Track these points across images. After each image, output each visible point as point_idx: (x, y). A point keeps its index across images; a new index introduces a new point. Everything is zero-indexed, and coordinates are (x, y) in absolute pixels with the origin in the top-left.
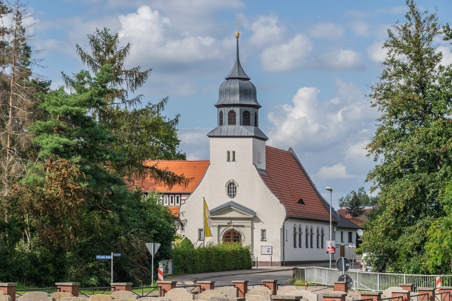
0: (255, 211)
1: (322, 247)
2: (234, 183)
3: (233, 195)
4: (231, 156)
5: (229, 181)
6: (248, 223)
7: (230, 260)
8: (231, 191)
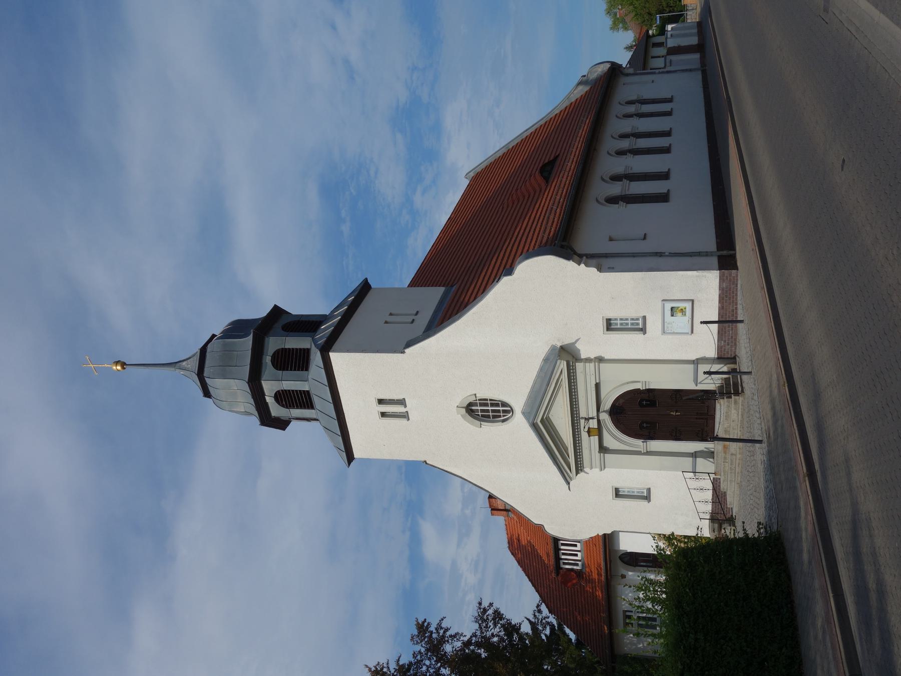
1: (670, 100)
4: (392, 408)
6: (585, 376)
8: (493, 411)
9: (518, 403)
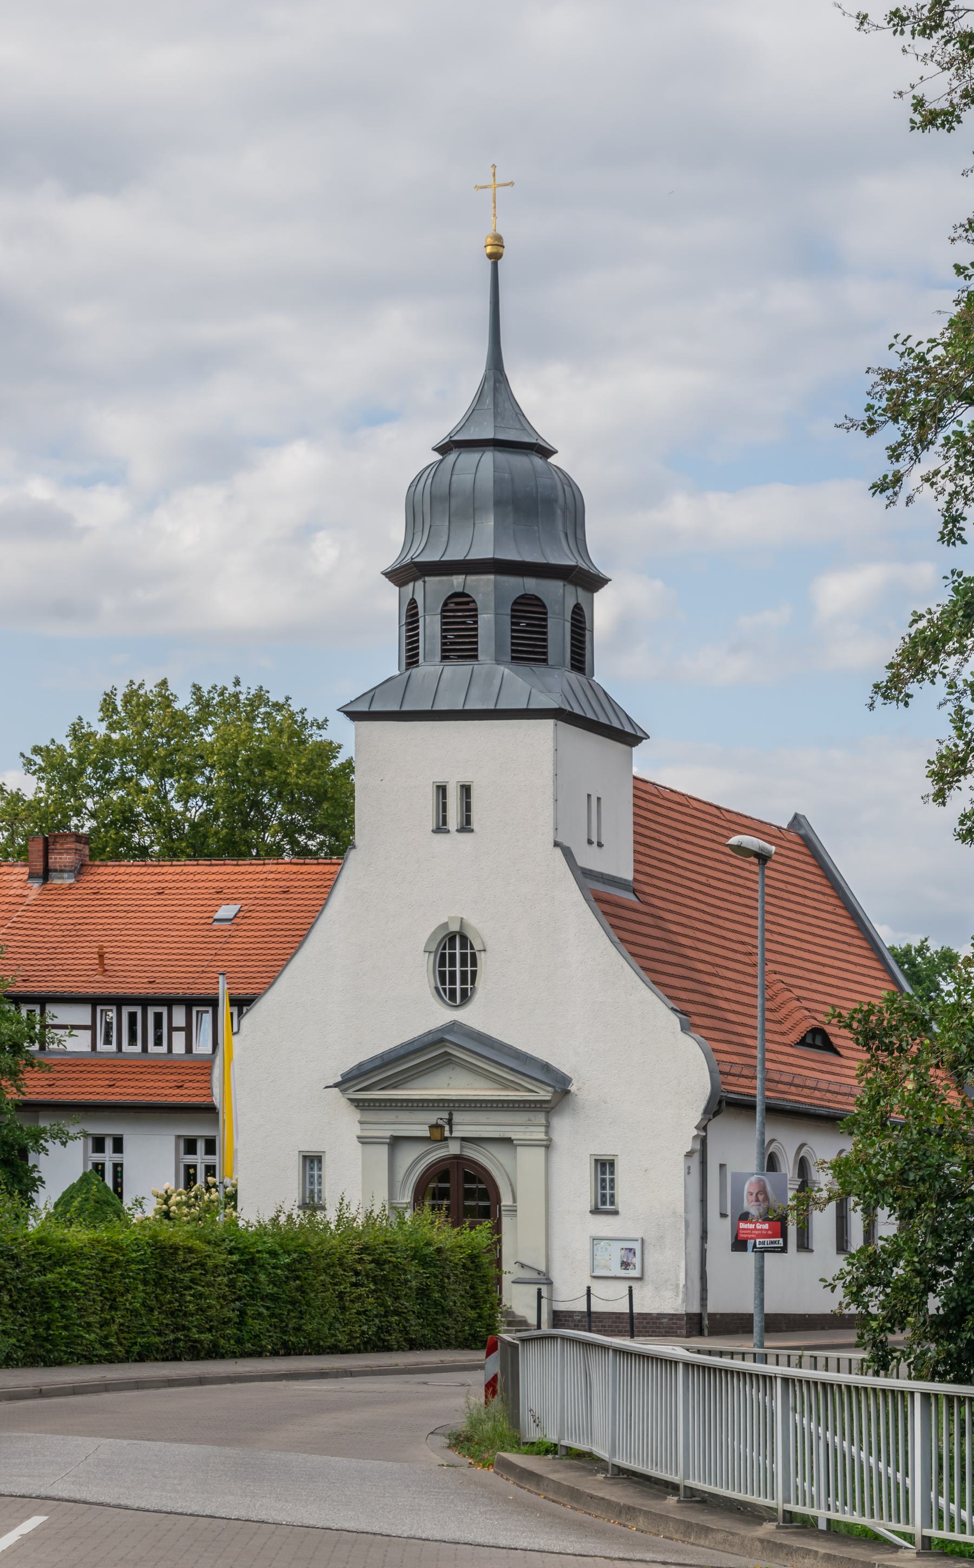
0: (565, 1070)
1: (442, 790)
2: (470, 936)
3: (464, 992)
5: (446, 924)
6: (522, 1129)
7: (341, 1296)
8: (453, 974)
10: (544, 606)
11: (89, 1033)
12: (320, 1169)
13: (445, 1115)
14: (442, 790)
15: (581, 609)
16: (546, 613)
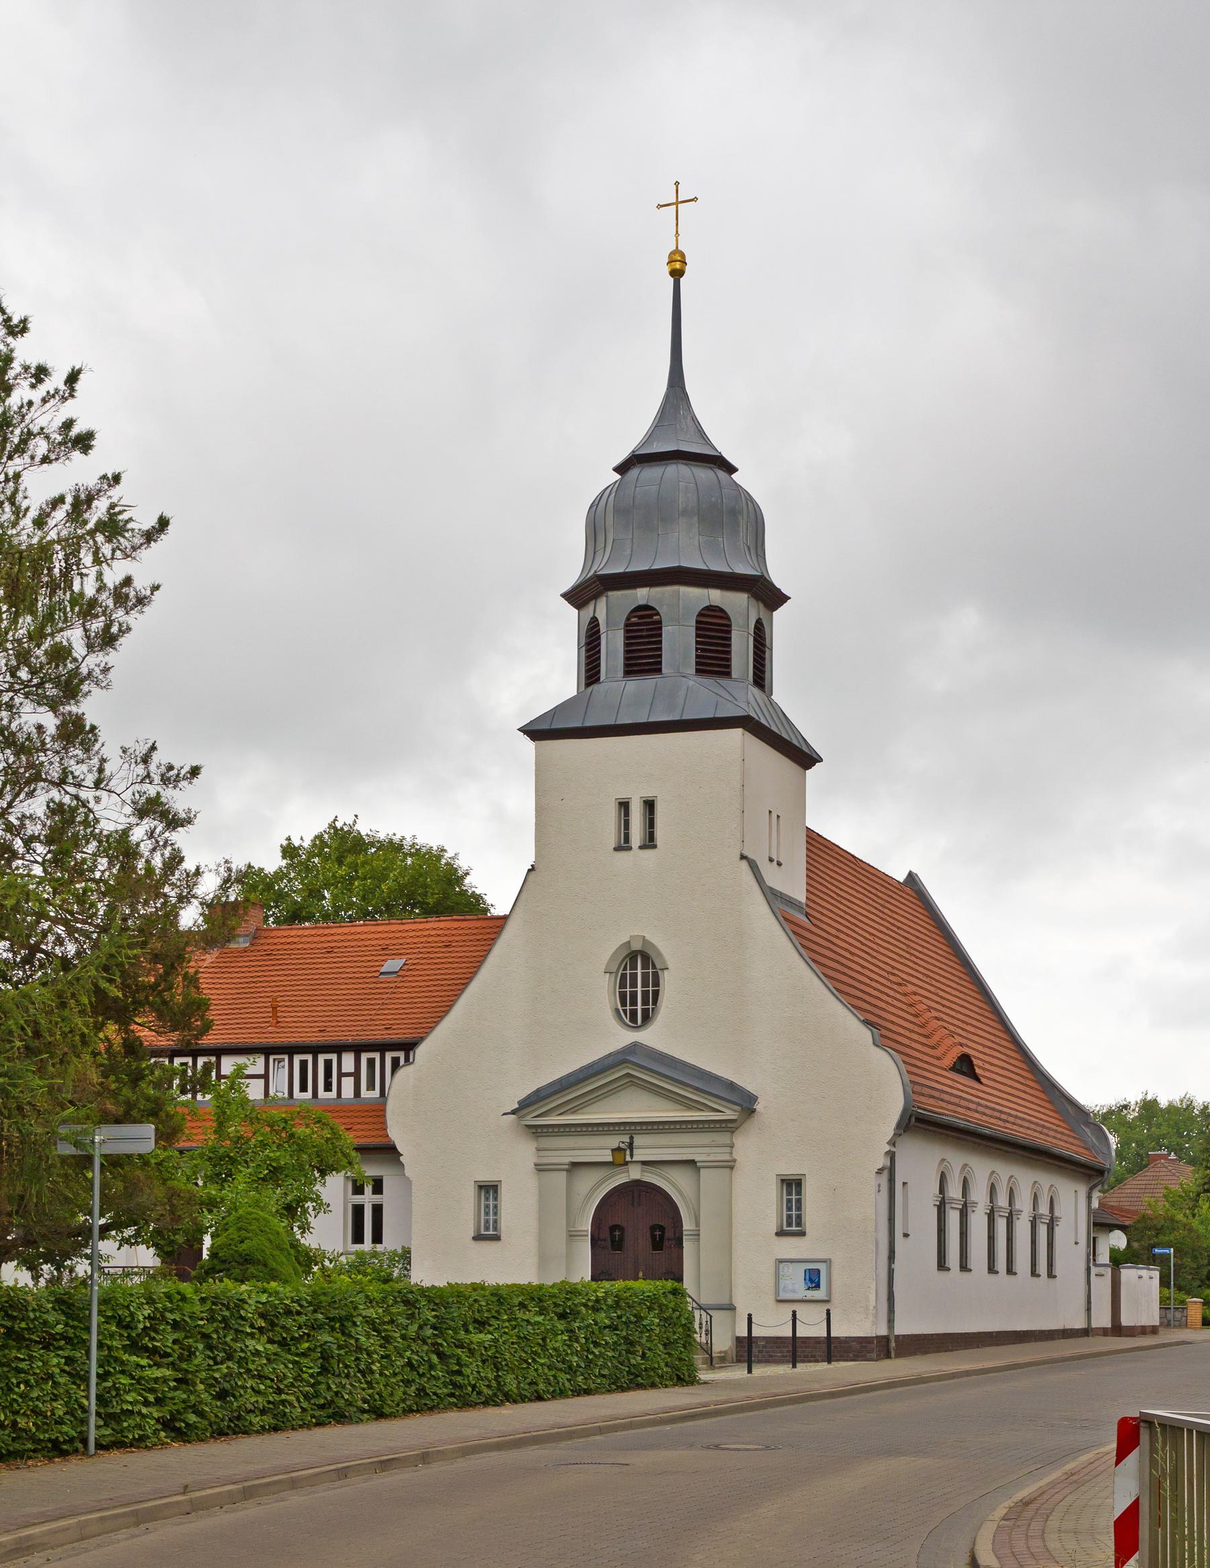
0: (750, 1088)
1: (1051, 1275)
9: (649, 1037)
10: (728, 619)
11: (262, 1081)
12: (496, 1199)
13: (626, 1139)
14: (624, 806)
15: (762, 625)
16: (730, 626)
